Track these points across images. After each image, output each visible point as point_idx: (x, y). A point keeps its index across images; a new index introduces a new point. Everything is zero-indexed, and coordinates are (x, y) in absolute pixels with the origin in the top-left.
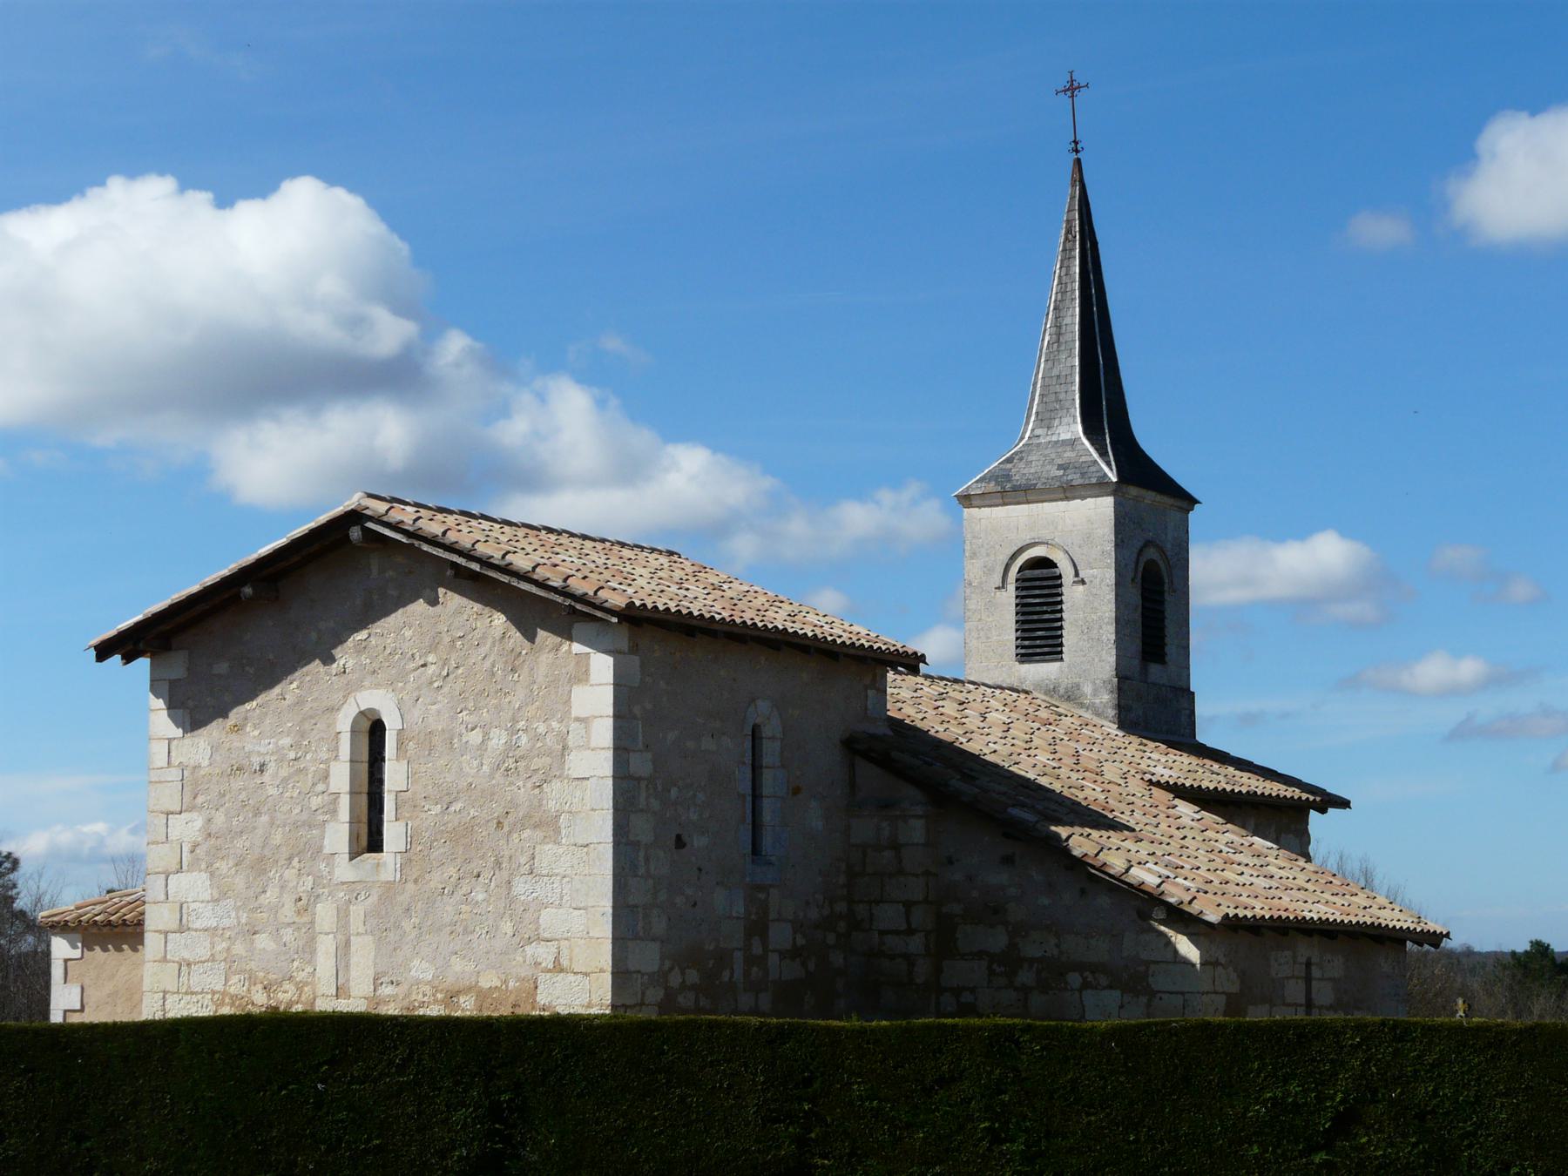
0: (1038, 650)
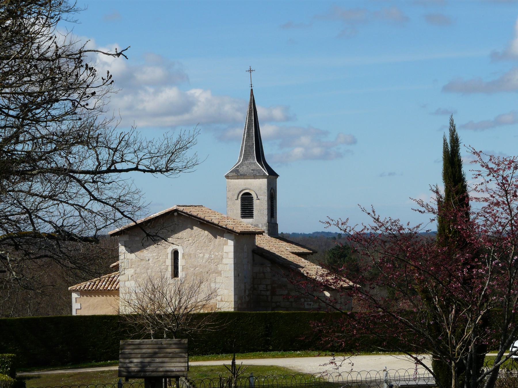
0: (247, 216)
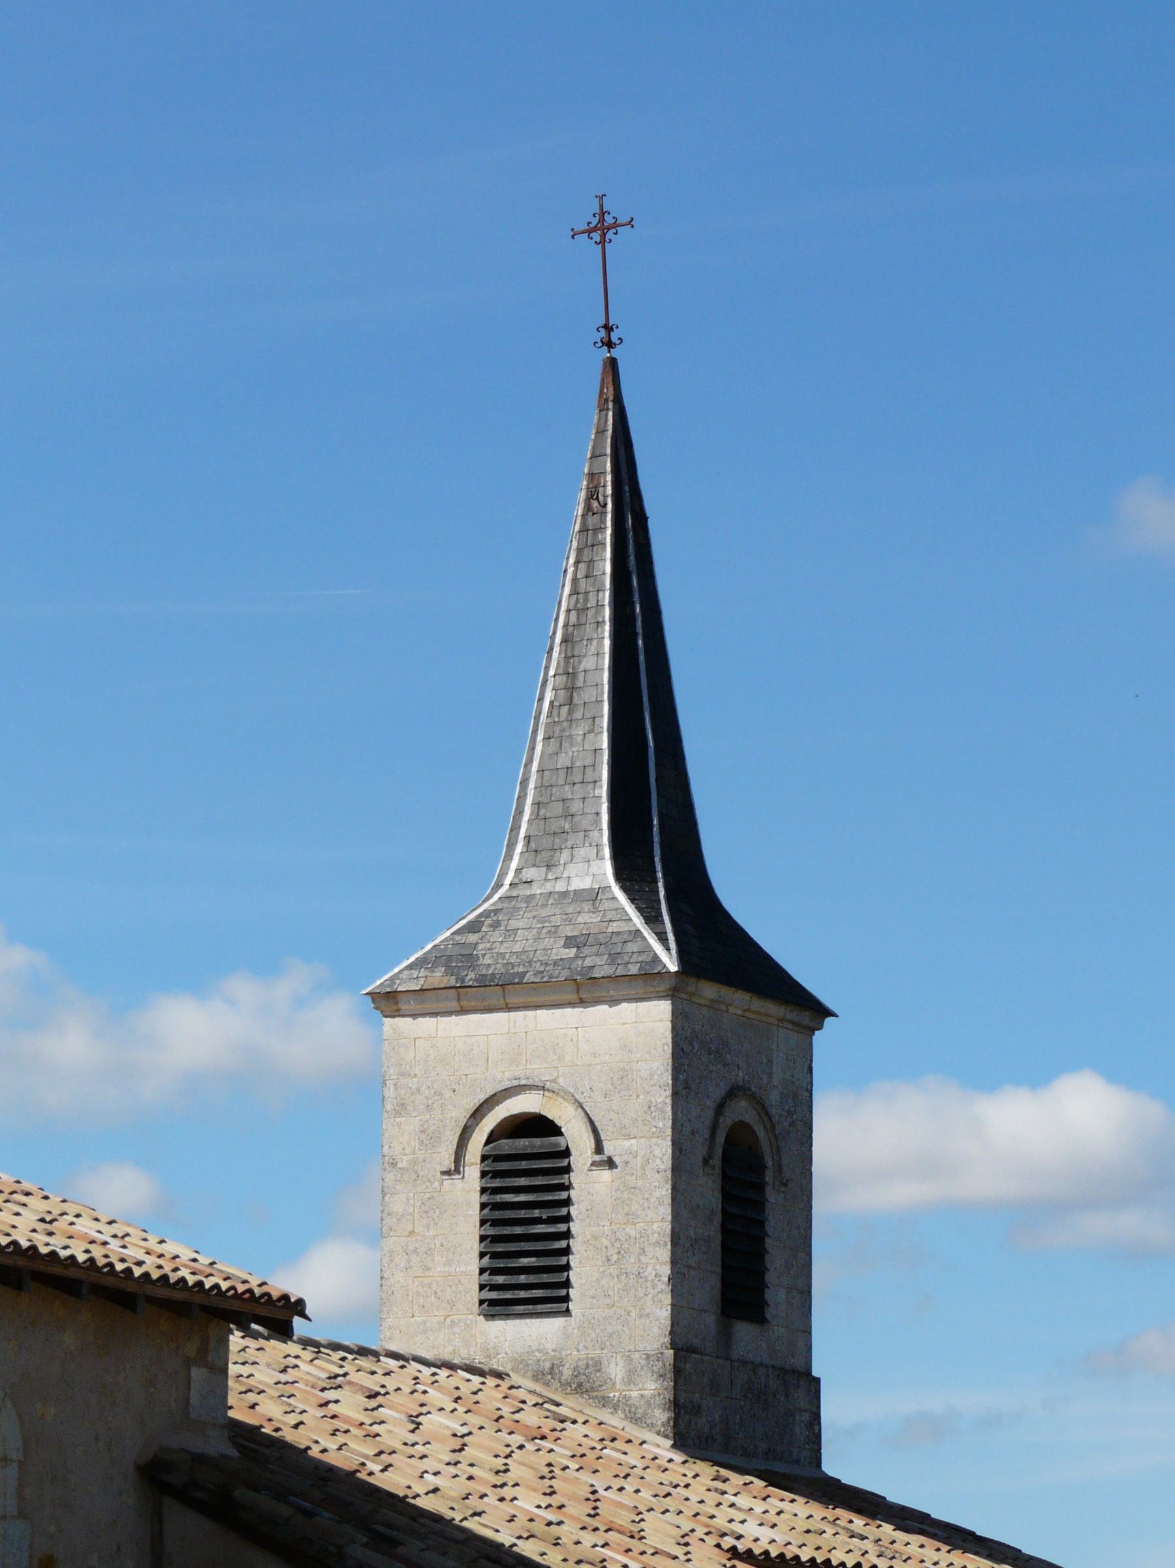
0: (523, 1294)
